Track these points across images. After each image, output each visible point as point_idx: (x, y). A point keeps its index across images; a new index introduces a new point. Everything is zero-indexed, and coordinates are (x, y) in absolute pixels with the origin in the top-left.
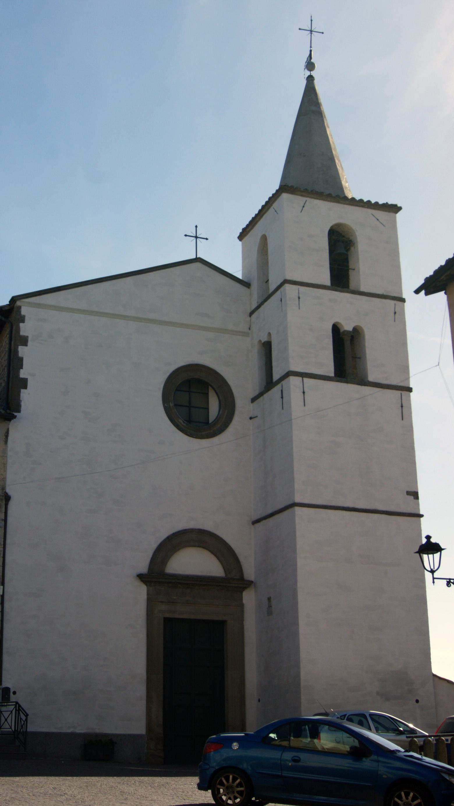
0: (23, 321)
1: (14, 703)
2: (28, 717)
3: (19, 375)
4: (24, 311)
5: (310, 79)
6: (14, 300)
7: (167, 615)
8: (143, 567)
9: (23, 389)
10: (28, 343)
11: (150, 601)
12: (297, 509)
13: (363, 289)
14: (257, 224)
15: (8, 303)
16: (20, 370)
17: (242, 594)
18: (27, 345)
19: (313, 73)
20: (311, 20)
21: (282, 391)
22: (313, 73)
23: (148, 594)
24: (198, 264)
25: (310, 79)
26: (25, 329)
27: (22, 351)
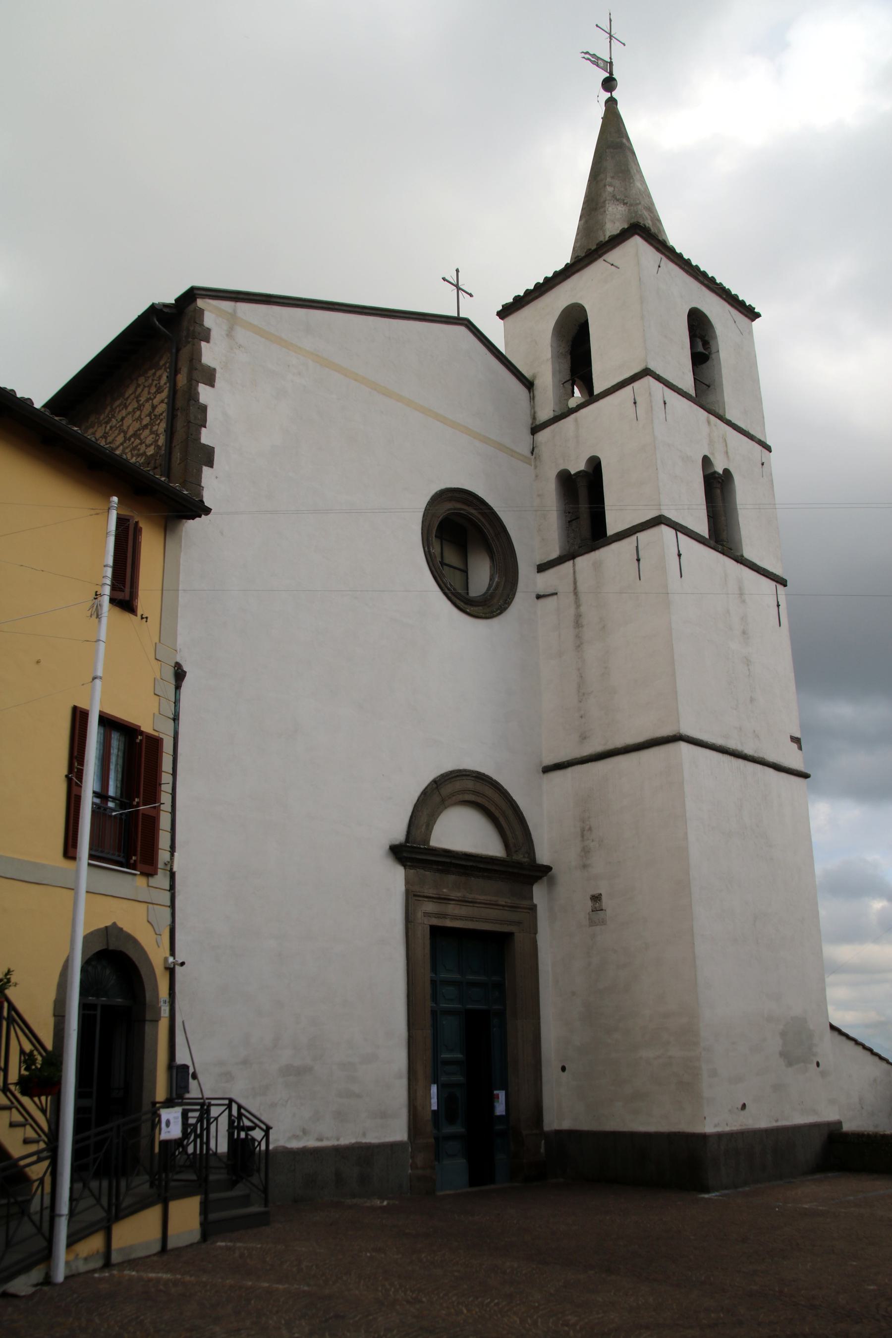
0: (207, 340)
1: (227, 1102)
2: (271, 1131)
3: (200, 439)
4: (209, 320)
5: (611, 104)
6: (191, 295)
7: (436, 922)
8: (398, 834)
9: (206, 466)
10: (215, 382)
11: (412, 897)
12: (683, 746)
13: (728, 416)
14: (658, 252)
15: (174, 302)
16: (201, 428)
17: (532, 888)
18: (214, 385)
19: (615, 94)
20: (610, 20)
21: (637, 547)
22: (615, 94)
23: (407, 882)
24: (462, 330)
25: (611, 104)
26: (210, 354)
27: (205, 393)
